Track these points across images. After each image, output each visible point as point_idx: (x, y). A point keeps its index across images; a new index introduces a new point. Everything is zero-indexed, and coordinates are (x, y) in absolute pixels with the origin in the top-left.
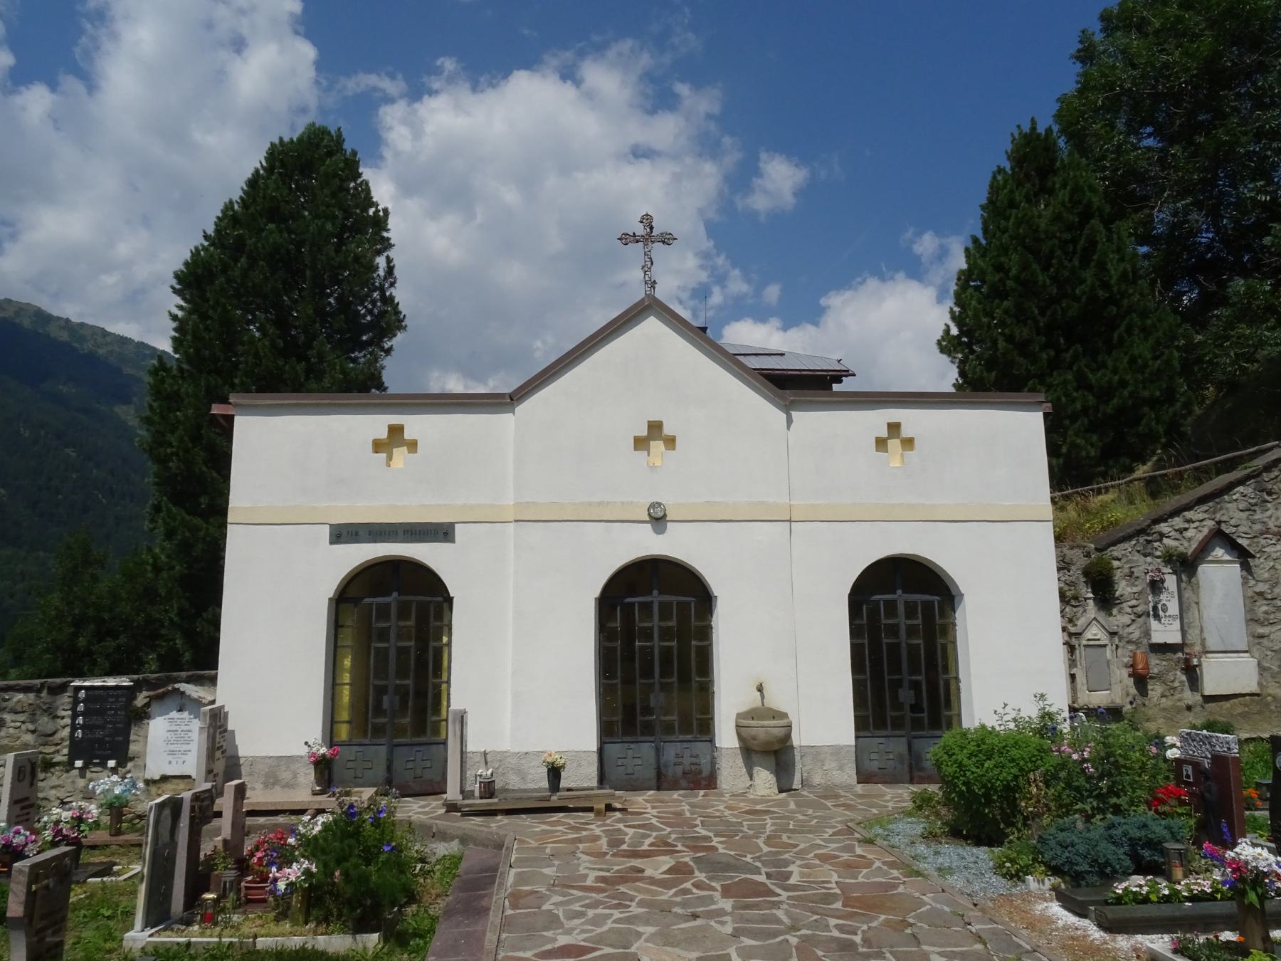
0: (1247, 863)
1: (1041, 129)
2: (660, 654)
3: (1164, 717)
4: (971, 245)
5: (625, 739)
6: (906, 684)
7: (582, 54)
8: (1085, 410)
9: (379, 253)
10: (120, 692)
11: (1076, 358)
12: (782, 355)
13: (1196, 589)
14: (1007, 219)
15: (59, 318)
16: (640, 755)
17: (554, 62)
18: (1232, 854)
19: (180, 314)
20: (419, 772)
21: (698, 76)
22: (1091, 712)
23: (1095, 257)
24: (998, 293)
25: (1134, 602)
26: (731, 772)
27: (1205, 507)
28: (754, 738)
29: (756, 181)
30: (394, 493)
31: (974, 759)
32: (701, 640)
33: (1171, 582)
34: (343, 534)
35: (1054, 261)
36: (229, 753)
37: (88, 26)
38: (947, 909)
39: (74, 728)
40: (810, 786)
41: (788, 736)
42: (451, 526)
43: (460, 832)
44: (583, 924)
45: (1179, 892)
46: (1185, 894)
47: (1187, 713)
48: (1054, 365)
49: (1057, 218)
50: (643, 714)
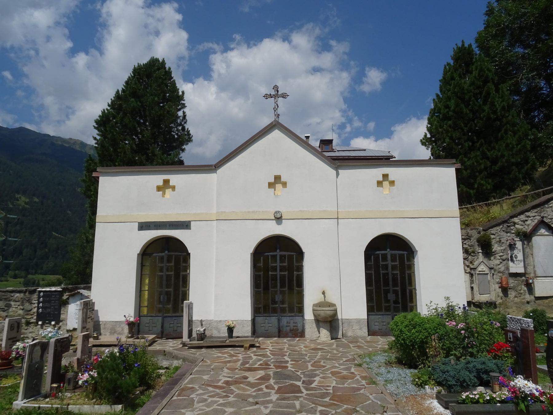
0: (520, 388)
1: (466, 45)
2: (280, 277)
3: (516, 307)
4: (435, 98)
5: (264, 315)
6: (391, 291)
7: (291, 31)
8: (486, 168)
9: (180, 110)
10: (57, 293)
11: (481, 145)
12: (365, 150)
13: (531, 248)
14: (450, 85)
15: (89, 145)
16: (270, 322)
17: (280, 34)
18: (513, 383)
19: (98, 137)
20: (175, 329)
21: (338, 36)
22: (479, 305)
23: (489, 100)
24: (446, 118)
25: (501, 254)
26: (311, 330)
27: (536, 210)
28: (319, 315)
29: (365, 79)
30: (165, 209)
31: (407, 328)
32: (298, 272)
33: (519, 245)
34: (143, 226)
35: (471, 103)
36: (95, 320)
37: (99, 29)
38: (379, 403)
39: (38, 308)
40: (346, 337)
41: (335, 314)
42: (189, 222)
43: (182, 356)
44: (203, 406)
45: (495, 398)
46: (498, 399)
47: (527, 305)
48: (471, 149)
49: (472, 84)
50: (272, 304)
